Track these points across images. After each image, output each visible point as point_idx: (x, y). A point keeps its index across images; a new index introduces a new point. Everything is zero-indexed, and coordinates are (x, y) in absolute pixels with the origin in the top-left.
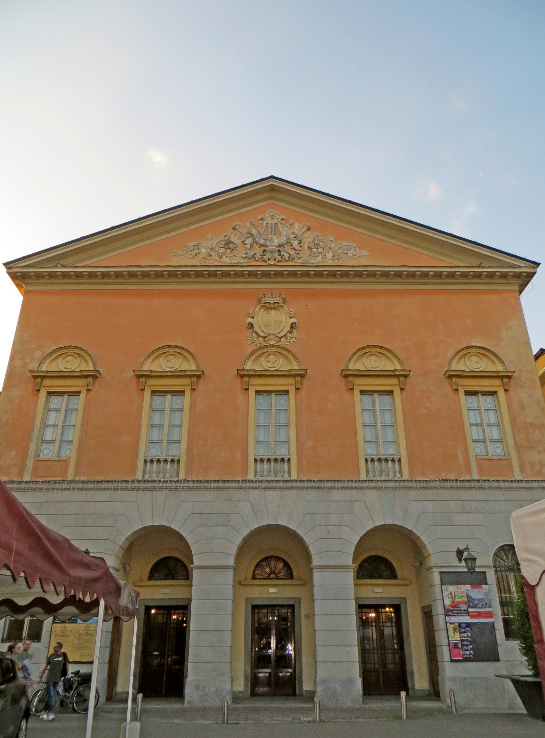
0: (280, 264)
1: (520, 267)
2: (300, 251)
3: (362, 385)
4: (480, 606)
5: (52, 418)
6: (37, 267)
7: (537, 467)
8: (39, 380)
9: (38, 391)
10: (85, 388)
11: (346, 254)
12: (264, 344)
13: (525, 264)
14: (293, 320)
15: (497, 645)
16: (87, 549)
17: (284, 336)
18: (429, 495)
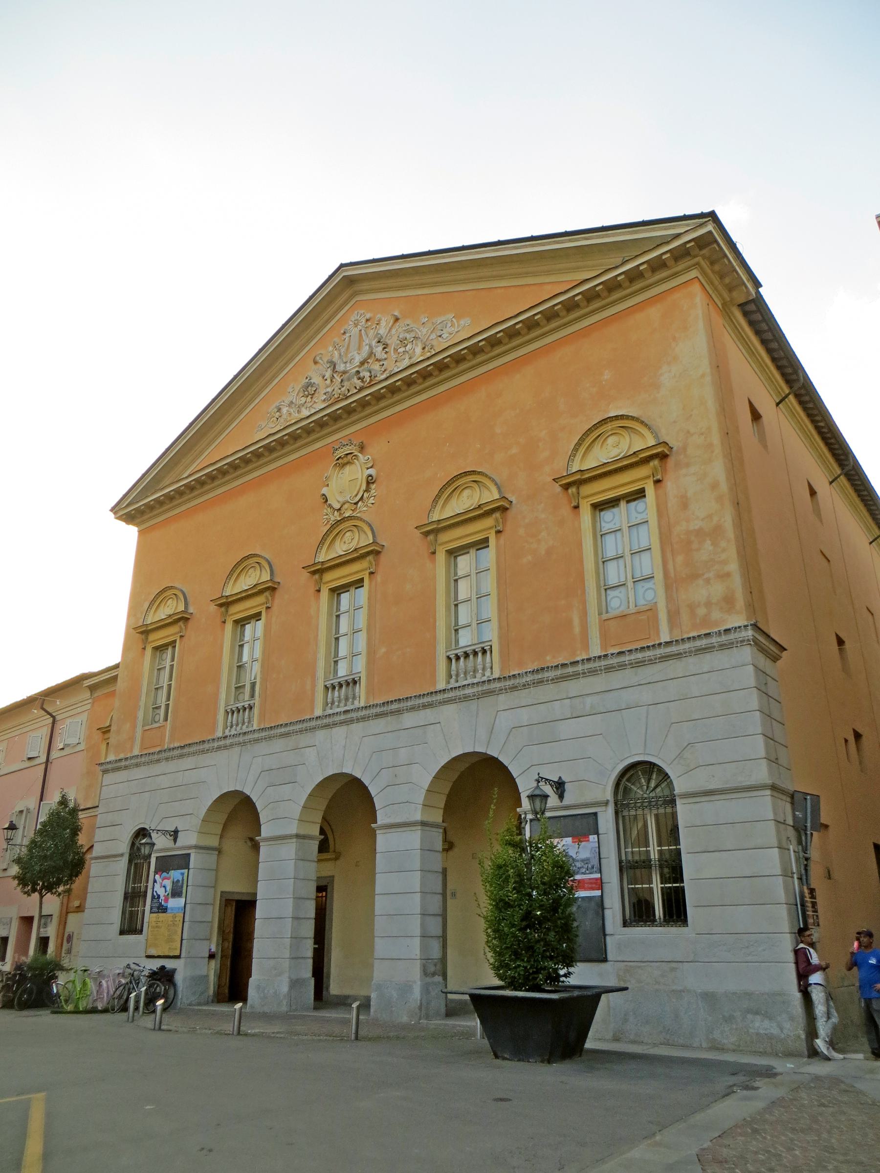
3: (447, 542)
4: (584, 870)
5: (611, 546)
7: (701, 611)
8: (572, 490)
9: (434, 553)
10: (493, 532)
11: (440, 336)
14: (371, 471)
15: (605, 935)
16: (560, 778)
18: (524, 696)
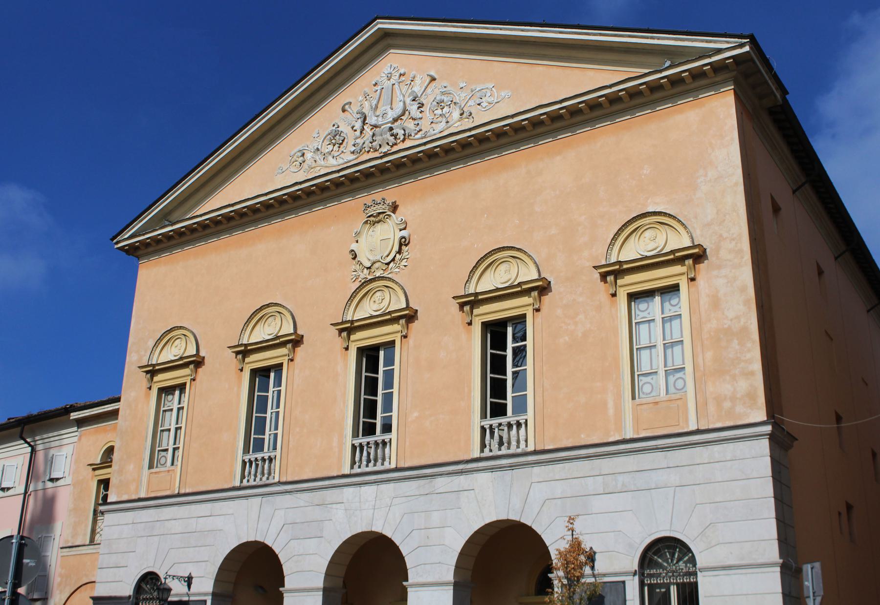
0: (395, 149)
1: (719, 51)
2: (421, 118)
6: (140, 235)
10: (531, 308)
11: (479, 104)
12: (370, 277)
13: (728, 42)
17: (393, 260)
